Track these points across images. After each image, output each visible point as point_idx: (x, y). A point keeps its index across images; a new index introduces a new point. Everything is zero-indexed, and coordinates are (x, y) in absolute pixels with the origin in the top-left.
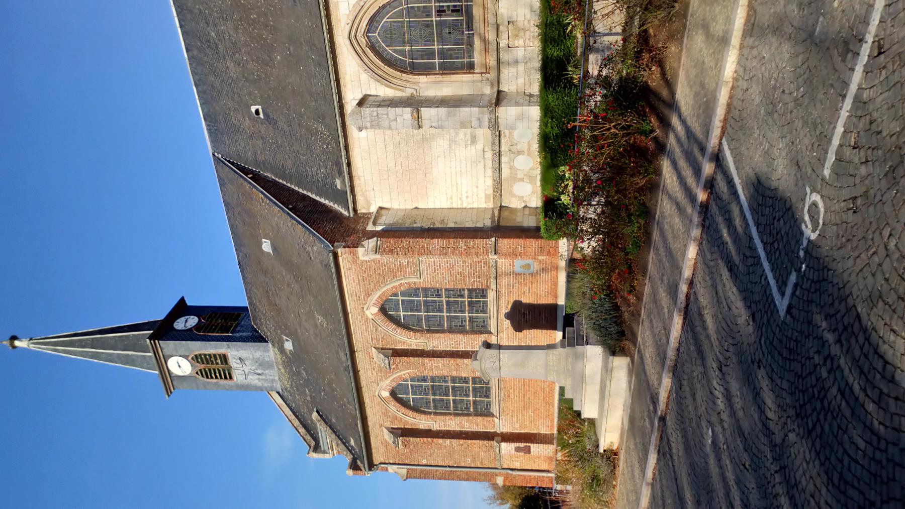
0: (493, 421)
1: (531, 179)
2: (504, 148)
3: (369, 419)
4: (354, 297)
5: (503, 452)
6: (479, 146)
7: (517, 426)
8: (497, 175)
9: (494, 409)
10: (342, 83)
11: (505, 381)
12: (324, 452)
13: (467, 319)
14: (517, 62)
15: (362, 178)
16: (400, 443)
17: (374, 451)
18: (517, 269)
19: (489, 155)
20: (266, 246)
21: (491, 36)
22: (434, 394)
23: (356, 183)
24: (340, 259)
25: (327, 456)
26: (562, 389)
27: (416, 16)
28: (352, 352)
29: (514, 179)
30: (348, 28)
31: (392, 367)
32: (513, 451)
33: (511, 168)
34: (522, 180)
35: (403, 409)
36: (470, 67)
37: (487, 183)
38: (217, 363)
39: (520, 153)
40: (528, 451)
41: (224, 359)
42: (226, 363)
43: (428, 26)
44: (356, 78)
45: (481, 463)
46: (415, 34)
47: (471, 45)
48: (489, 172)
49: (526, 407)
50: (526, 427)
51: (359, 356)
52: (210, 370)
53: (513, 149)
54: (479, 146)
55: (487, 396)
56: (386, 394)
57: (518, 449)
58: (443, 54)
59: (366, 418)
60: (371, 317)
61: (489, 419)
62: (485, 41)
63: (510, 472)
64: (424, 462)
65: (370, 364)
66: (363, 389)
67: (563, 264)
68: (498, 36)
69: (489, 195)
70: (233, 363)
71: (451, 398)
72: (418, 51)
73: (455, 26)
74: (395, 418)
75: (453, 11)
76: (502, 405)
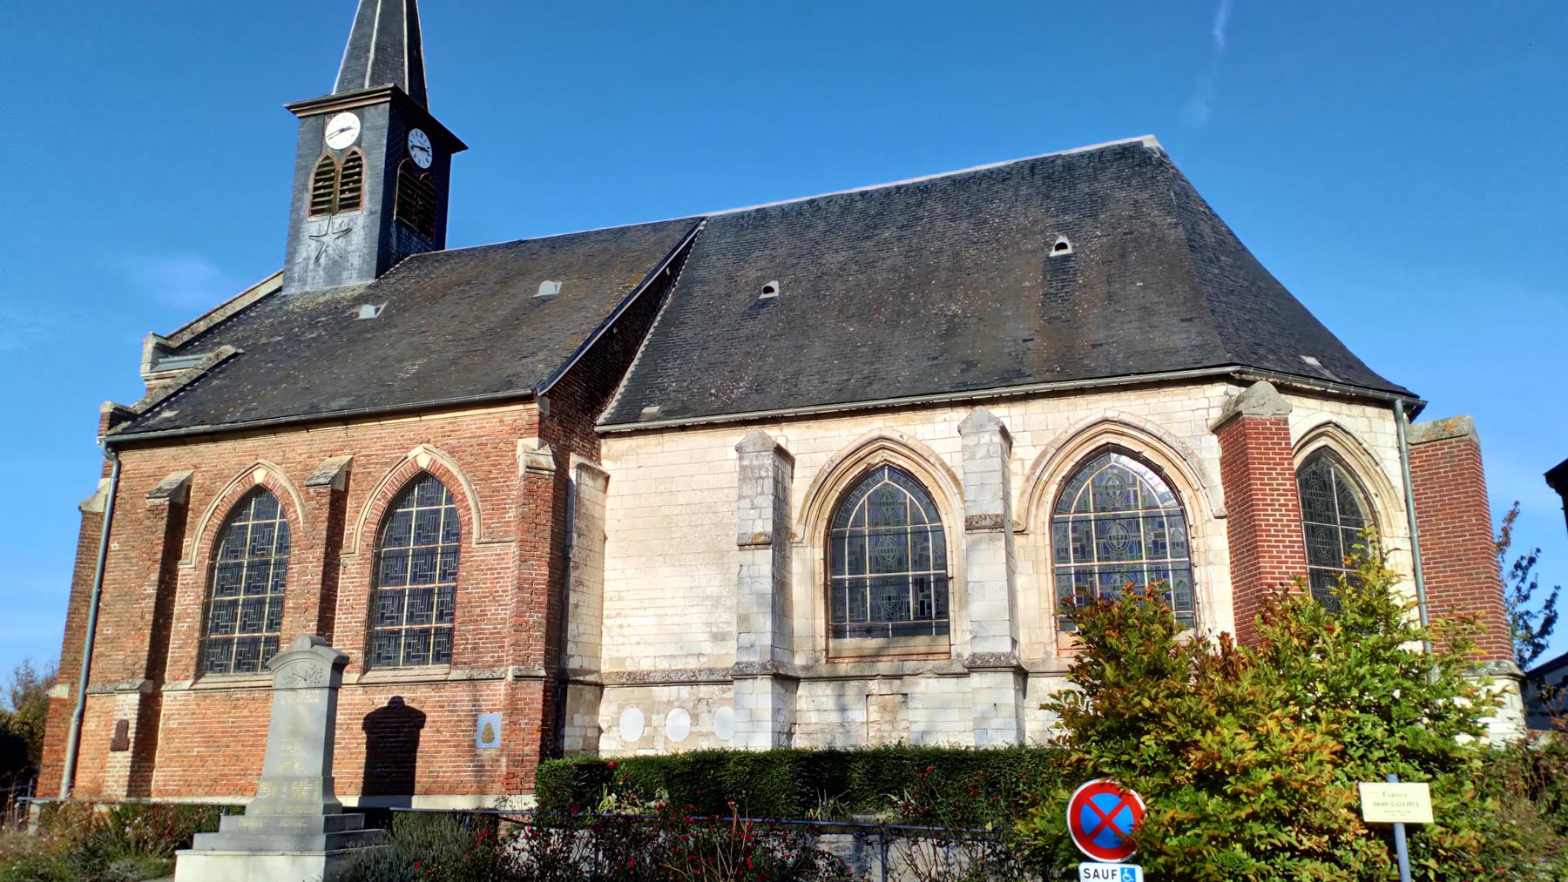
0: (187, 678)
1: (648, 740)
2: (704, 690)
3: (212, 446)
4: (450, 427)
5: (120, 697)
6: (707, 647)
7: (173, 724)
8: (658, 679)
9: (211, 680)
10: (811, 423)
11: (266, 700)
12: (154, 363)
13: (396, 628)
14: (843, 709)
15: (659, 449)
16: (157, 501)
17: (147, 453)
18: (484, 719)
19: (693, 664)
20: (548, 288)
21: (884, 666)
22: (251, 566)
23: (652, 439)
24: (520, 407)
25: (145, 368)
26: (241, 810)
27: (914, 544)
28: (345, 420)
29: (650, 710)
30: (896, 436)
31: (311, 490)
32: (119, 716)
33: (670, 703)
34: (648, 723)
35: (225, 508)
36: (836, 632)
37: (645, 661)
38: (342, 192)
39: (695, 718)
40: (119, 745)
41: (352, 204)
42: (342, 207)
43: (900, 562)
44: (822, 446)
45: (102, 655)
46: (887, 543)
47: (868, 632)
48: (664, 665)
49: (211, 740)
50: (168, 740)
51: (337, 433)
52: (332, 179)
53: (702, 707)
54: (707, 647)
55: (238, 666)
56: (259, 477)
57: (123, 726)
58: (857, 586)
59: (214, 441)
60: (411, 455)
61: (192, 670)
62: (876, 655)
63: (76, 712)
64: (114, 546)
65: (323, 450)
66: (273, 437)
67: (489, 802)
68: (885, 677)
69: (623, 665)
70: (342, 219)
71: (242, 597)
72: (863, 547)
73: (899, 606)
74: (210, 494)
75: (922, 603)
76: (218, 695)
